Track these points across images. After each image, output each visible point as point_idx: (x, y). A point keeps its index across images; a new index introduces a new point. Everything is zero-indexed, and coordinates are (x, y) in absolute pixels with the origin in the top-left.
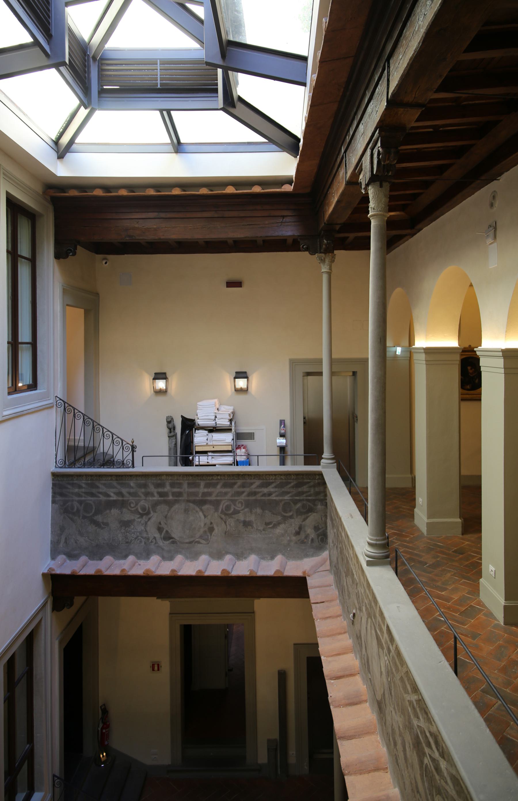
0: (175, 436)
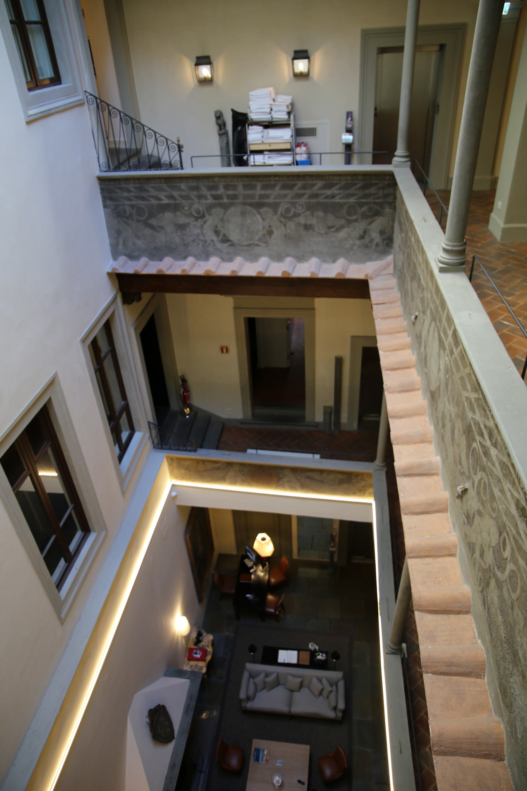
0: (226, 133)
